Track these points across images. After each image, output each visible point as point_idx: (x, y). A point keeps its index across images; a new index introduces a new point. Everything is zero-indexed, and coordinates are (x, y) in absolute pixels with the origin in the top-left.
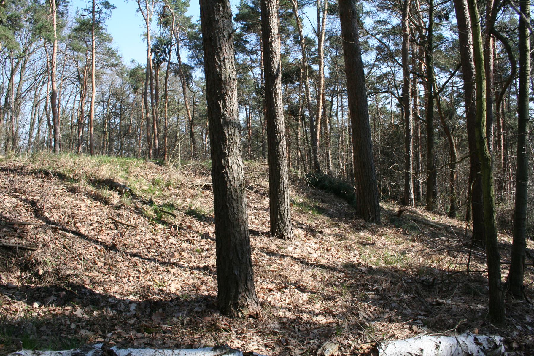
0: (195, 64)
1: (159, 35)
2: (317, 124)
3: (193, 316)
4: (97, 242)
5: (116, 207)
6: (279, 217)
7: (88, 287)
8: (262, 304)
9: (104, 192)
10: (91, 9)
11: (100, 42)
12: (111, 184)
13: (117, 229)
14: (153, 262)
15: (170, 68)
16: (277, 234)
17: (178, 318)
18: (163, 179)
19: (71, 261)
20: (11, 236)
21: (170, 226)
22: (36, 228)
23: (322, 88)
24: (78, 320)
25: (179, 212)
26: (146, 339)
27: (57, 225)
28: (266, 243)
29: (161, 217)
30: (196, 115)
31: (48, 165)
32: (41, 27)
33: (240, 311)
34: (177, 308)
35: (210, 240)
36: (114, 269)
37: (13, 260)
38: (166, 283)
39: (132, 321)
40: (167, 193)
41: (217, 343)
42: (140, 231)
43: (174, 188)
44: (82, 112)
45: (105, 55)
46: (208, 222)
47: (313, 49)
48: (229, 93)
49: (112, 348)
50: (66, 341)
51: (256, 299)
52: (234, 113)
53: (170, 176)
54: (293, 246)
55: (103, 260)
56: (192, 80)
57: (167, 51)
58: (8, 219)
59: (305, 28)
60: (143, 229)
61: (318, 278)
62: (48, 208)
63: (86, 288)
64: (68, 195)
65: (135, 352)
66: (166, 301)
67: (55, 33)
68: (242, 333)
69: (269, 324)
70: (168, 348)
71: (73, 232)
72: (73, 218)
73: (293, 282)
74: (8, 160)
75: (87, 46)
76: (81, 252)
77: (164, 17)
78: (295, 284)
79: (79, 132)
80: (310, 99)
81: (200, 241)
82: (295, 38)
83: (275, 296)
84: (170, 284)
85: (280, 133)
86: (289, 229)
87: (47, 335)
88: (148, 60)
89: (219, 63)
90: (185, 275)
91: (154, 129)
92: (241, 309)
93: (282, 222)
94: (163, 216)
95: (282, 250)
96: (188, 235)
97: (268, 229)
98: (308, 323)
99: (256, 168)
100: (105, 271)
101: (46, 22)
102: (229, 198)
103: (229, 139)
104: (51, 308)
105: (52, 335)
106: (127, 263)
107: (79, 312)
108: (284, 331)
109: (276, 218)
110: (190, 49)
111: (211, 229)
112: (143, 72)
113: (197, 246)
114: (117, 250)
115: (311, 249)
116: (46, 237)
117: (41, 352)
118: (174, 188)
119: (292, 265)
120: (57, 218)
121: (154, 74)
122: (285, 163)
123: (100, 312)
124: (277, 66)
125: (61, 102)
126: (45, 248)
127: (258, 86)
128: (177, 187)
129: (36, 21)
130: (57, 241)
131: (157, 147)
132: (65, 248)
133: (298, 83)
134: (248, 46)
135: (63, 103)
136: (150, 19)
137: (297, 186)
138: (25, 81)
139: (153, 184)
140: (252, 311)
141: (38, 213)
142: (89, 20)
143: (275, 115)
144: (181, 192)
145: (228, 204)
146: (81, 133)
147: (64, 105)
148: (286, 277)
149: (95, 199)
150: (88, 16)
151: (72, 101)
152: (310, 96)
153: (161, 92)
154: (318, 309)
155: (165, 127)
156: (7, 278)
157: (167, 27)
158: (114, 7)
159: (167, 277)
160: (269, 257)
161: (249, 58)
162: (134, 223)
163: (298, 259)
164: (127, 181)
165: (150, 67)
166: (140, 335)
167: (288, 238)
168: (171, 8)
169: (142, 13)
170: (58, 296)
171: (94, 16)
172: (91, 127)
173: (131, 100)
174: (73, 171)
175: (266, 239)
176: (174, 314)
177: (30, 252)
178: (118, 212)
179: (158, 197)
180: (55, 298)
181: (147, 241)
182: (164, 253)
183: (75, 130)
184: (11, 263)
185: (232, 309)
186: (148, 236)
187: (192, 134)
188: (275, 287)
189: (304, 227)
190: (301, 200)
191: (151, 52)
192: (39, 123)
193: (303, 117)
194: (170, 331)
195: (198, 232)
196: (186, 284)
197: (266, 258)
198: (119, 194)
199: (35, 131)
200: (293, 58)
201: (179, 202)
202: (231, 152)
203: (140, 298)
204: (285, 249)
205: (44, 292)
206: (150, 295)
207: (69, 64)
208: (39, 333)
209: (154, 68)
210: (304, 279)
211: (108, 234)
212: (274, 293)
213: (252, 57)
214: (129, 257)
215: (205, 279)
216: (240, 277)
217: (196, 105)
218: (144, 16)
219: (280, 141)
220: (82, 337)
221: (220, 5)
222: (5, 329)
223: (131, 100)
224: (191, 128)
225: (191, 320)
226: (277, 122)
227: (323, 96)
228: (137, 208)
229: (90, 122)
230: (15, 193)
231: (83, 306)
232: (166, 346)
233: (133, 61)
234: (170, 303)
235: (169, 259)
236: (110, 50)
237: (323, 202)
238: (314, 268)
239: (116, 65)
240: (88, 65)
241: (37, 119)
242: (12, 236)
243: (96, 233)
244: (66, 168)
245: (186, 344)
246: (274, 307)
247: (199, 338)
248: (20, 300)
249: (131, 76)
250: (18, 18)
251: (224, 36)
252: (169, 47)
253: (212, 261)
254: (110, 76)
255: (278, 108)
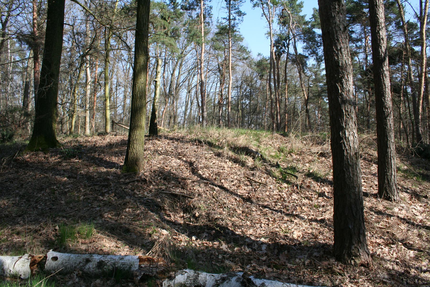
0: (309, 54)
1: (279, 32)
2: (419, 99)
3: (313, 259)
4: (237, 195)
5: (251, 168)
6: (386, 181)
7: (230, 229)
8: (372, 256)
9: (241, 156)
10: (228, 18)
11: (235, 42)
12: (247, 151)
13: (251, 185)
14: (279, 213)
15: (289, 58)
16: (384, 196)
17: (300, 259)
18: (286, 147)
19: (218, 208)
20: (177, 187)
21: (293, 185)
22: (193, 182)
23: (424, 67)
24: (224, 253)
25: (300, 175)
26: (275, 273)
27: (208, 180)
28: (374, 203)
29: (286, 177)
30: (311, 95)
31: (201, 136)
32: (193, 35)
33: (353, 259)
34: (299, 251)
35: (325, 198)
36: (250, 216)
37: (178, 204)
38: (290, 231)
39: (264, 258)
40: (290, 158)
41: (333, 284)
42: (269, 188)
43: (296, 155)
44: (222, 95)
45: (238, 51)
46: (324, 183)
47: (415, 33)
48: (346, 76)
49: (250, 277)
50: (216, 267)
51: (367, 251)
52: (350, 93)
53: (292, 145)
54: (399, 207)
55: (241, 209)
56: (306, 67)
57: (286, 45)
58: (174, 174)
59: (406, 14)
60: (272, 186)
61: (424, 238)
62: (201, 168)
63: (229, 229)
64: (215, 158)
65: (267, 283)
66: (290, 245)
67: (203, 38)
68: (354, 278)
69: (379, 274)
70: (294, 283)
71: (219, 186)
72: (219, 176)
73: (400, 239)
74: (173, 132)
75: (225, 46)
76: (225, 201)
77: (283, 18)
78: (402, 241)
79: (219, 111)
80: (412, 77)
81: (318, 199)
82: (397, 24)
83: (383, 250)
84: (293, 232)
85: (387, 109)
86: (396, 193)
87: (203, 261)
88: (271, 53)
89: (337, 52)
90: (305, 225)
91: (277, 107)
92: (353, 258)
93: (389, 186)
94: (287, 177)
95: (389, 211)
96: (307, 193)
97: (376, 192)
98: (416, 278)
99: (363, 139)
100: (243, 218)
101: (196, 31)
102: (346, 164)
103: (346, 114)
104: (204, 242)
105: (206, 261)
106: (259, 213)
107: (224, 246)
108: (393, 282)
109: (384, 182)
110: (304, 42)
111: (327, 189)
112: (267, 62)
113: (315, 202)
114: (252, 202)
115: (416, 211)
116: (200, 189)
117: (199, 272)
118: (296, 155)
119: (398, 224)
120: (208, 175)
121: (276, 64)
122: (392, 135)
123: (239, 248)
124: (384, 51)
125: (207, 88)
126: (200, 197)
127: (363, 69)
128: (298, 154)
129: (190, 31)
130: (208, 192)
131: (279, 122)
132: (214, 198)
133: (400, 64)
134: (354, 36)
135: (208, 89)
136: (272, 21)
137: (403, 155)
138: (182, 74)
139: (279, 151)
140: (364, 261)
141: (194, 171)
142: (226, 26)
143: (383, 93)
144: (301, 158)
145: (344, 169)
146: (221, 112)
147: (209, 91)
148: (393, 235)
149: (235, 162)
150: (225, 23)
151: (214, 87)
152: (412, 74)
153: (282, 78)
154: (425, 266)
155: (286, 106)
156: (174, 217)
157: (285, 26)
158: (244, 14)
159: (292, 226)
160: (377, 215)
161: (354, 45)
162: (265, 182)
163: (404, 219)
164: (258, 149)
165: (273, 58)
166: (270, 269)
167: (395, 200)
168: (289, 10)
169: (266, 16)
170: (209, 234)
171: (230, 22)
172: (228, 107)
173: (258, 85)
174: (218, 140)
175: (374, 200)
176: (297, 256)
177: (189, 199)
178: (252, 172)
179: (283, 161)
180: (207, 235)
181: (275, 196)
182: (288, 206)
183: (217, 110)
184: (177, 206)
185: (346, 257)
186: (275, 192)
187: (307, 111)
188: (383, 242)
189: (408, 191)
190: (406, 167)
191: (274, 47)
192: (191, 105)
193: (406, 93)
194: (294, 270)
195: (315, 191)
196: (306, 233)
197: (375, 216)
198: (253, 159)
199: (189, 111)
200: (396, 42)
201: (300, 166)
202: (347, 126)
203: (269, 241)
204: (391, 209)
205: (199, 229)
206: (277, 239)
207: (212, 60)
208: (197, 259)
209: (276, 58)
210: (410, 238)
211: (245, 189)
212: (383, 247)
213: (357, 44)
214: (261, 208)
215: (321, 230)
216: (354, 230)
217: (310, 87)
218: (267, 19)
219: (388, 116)
220: (227, 266)
221: (336, 4)
222: (175, 253)
223: (258, 85)
224: (307, 107)
225: (311, 263)
226: (384, 99)
227: (425, 75)
228: (266, 170)
229: (228, 103)
230: (179, 156)
231: (227, 243)
232: (291, 281)
233: (259, 54)
234: (293, 247)
235: (292, 212)
236: (241, 47)
237: (426, 169)
238: (420, 228)
239: (247, 58)
240: (225, 59)
241: (190, 102)
242: (177, 187)
243: (236, 188)
244: (213, 138)
245: (307, 281)
246: (382, 259)
247: (318, 278)
248: (183, 233)
249: (258, 66)
250: (177, 30)
251: (340, 29)
252: (287, 41)
253: (329, 215)
254: (242, 67)
255: (385, 88)
